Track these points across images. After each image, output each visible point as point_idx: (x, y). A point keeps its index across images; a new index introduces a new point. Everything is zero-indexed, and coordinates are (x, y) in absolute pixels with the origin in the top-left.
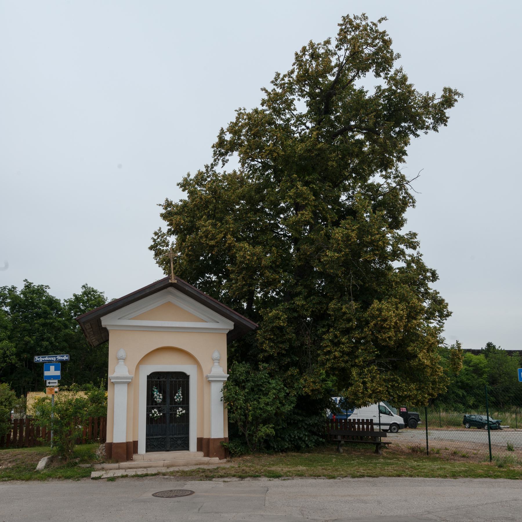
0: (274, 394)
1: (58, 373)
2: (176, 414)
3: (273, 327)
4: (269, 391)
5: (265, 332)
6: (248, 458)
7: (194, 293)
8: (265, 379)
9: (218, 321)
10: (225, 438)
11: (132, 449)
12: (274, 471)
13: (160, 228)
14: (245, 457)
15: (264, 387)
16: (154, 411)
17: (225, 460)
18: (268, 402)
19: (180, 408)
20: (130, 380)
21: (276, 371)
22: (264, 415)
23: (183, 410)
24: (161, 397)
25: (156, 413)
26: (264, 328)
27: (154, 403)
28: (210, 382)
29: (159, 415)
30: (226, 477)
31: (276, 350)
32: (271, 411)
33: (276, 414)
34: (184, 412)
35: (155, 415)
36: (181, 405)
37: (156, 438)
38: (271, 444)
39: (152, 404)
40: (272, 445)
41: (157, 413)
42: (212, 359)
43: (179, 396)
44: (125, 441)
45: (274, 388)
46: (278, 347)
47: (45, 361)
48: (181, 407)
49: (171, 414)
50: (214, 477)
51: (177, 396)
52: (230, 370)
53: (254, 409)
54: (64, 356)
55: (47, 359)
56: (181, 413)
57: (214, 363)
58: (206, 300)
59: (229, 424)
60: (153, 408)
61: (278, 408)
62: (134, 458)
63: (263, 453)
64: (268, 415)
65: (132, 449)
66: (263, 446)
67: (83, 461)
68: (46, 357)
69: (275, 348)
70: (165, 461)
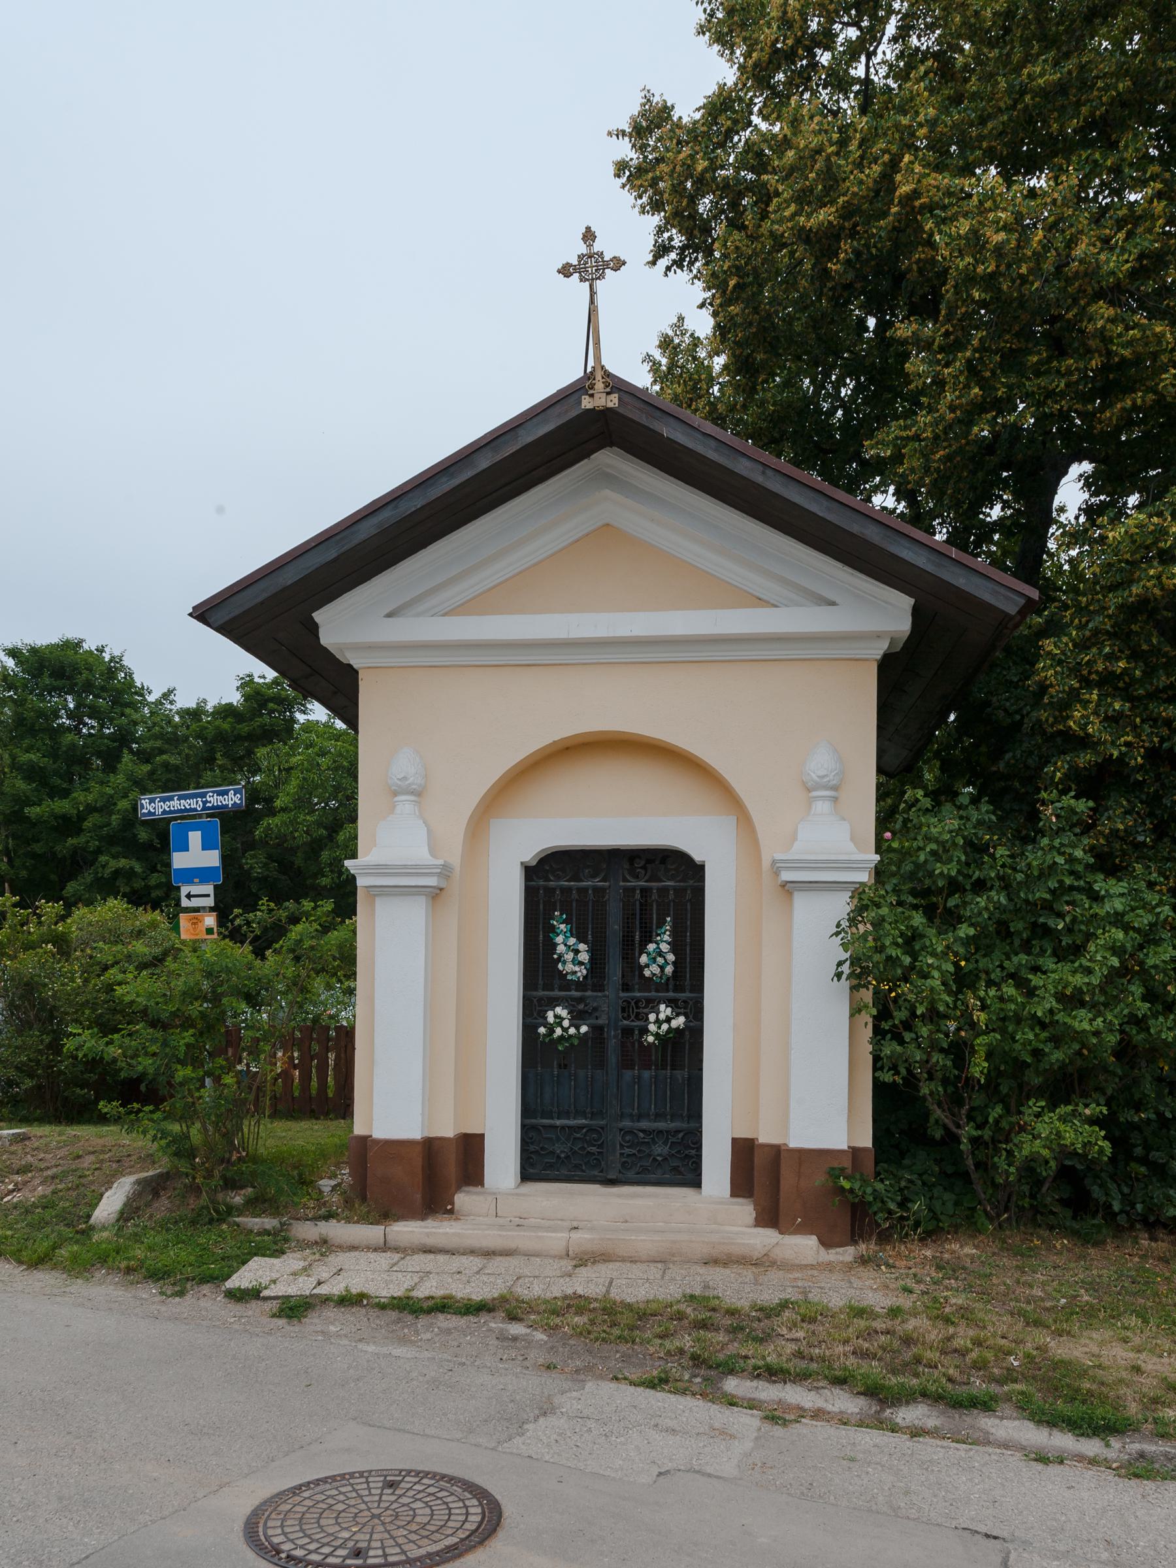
0: (1117, 950)
1: (212, 859)
2: (646, 1031)
3: (1132, 611)
4: (1089, 936)
5: (1082, 646)
6: (969, 1250)
7: (700, 448)
8: (1072, 873)
9: (831, 596)
10: (855, 1152)
11: (451, 1166)
12: (1083, 1373)
13: (681, 319)
14: (955, 1246)
15: (1061, 915)
16: (556, 1016)
17: (851, 1250)
18: (1078, 991)
19: (662, 1007)
20: (432, 881)
21: (1138, 846)
22: (1057, 1056)
23: (678, 1015)
24: (584, 957)
25: (560, 1024)
26: (1080, 627)
27: (557, 982)
28: (788, 889)
29: (572, 1031)
30: (801, 1377)
31: (1138, 736)
32: (1097, 1033)
33: (1124, 1051)
34: (679, 1022)
35: (558, 1031)
36: (671, 994)
37: (563, 1128)
38: (1095, 1188)
39: (548, 987)
40: (1096, 1192)
41: (566, 1023)
42: (804, 783)
43: (660, 954)
44: (416, 1134)
45: (1118, 919)
46: (1154, 720)
47: (171, 812)
48: (670, 1003)
49: (627, 1032)
50: (731, 1372)
51: (648, 954)
52: (888, 835)
53: (1003, 1023)
54: (226, 793)
55: (175, 804)
56: (665, 1027)
57: (810, 801)
58: (759, 479)
59: (879, 1088)
60: (552, 1003)
61: (1139, 1022)
62: (457, 1207)
63: (1051, 1228)
64: (1079, 1053)
65: (451, 1166)
66: (1049, 1196)
67: (259, 1204)
68: (171, 799)
69: (1135, 727)
70: (575, 1235)
